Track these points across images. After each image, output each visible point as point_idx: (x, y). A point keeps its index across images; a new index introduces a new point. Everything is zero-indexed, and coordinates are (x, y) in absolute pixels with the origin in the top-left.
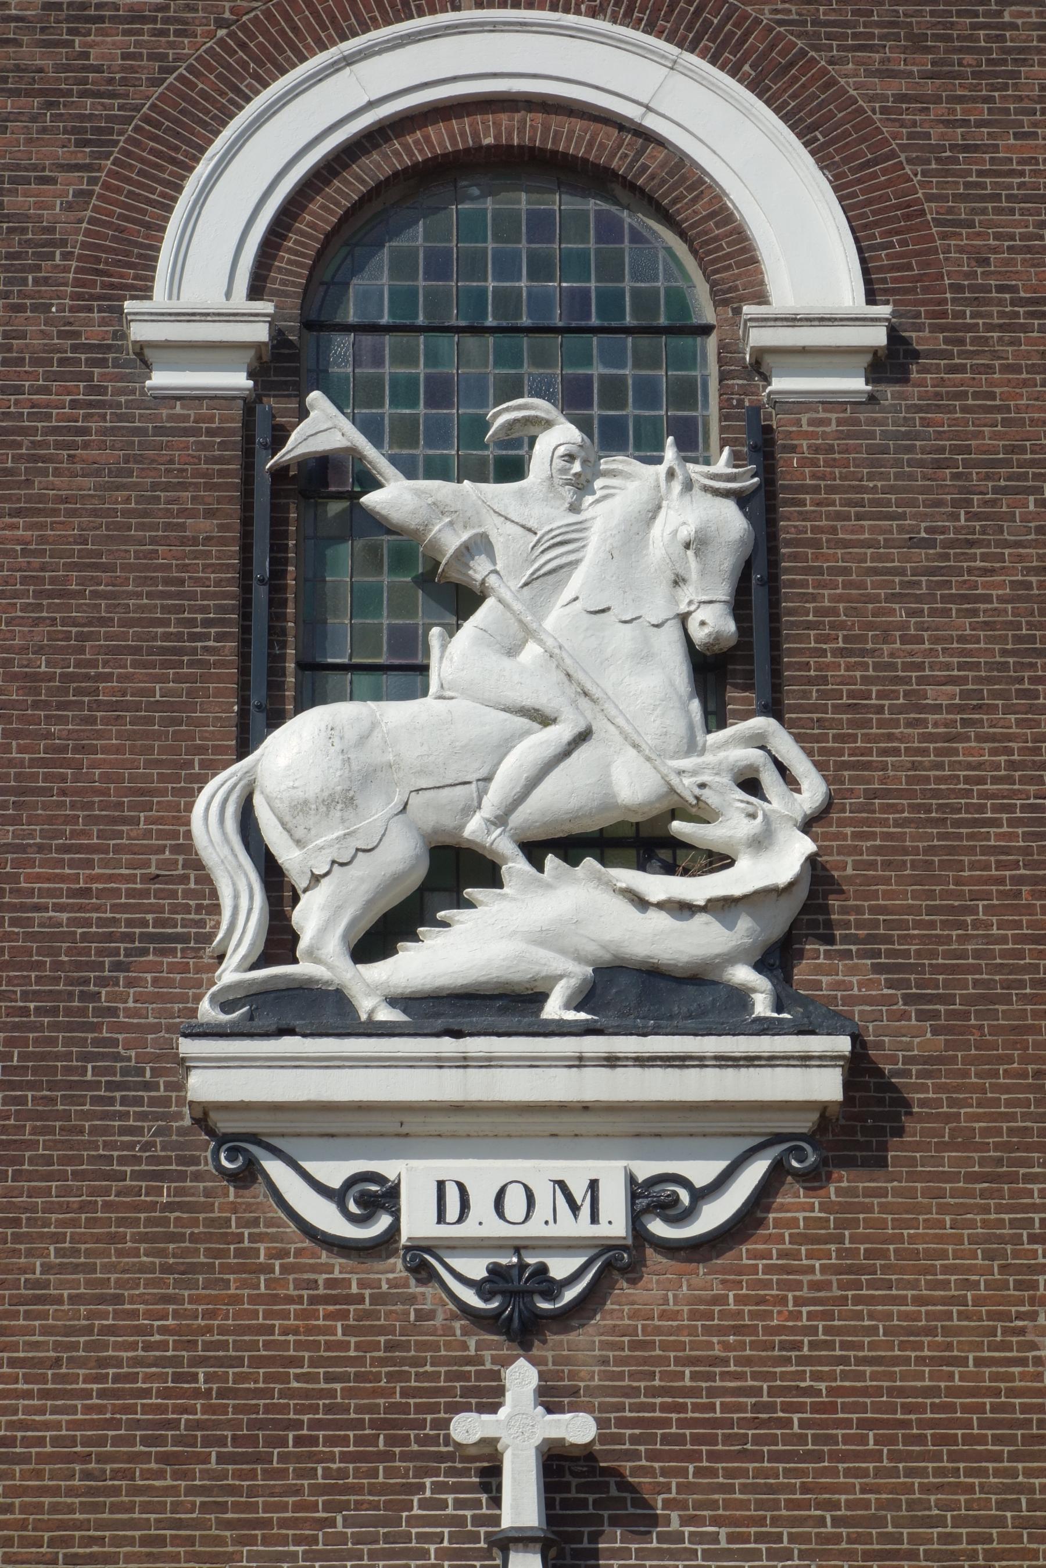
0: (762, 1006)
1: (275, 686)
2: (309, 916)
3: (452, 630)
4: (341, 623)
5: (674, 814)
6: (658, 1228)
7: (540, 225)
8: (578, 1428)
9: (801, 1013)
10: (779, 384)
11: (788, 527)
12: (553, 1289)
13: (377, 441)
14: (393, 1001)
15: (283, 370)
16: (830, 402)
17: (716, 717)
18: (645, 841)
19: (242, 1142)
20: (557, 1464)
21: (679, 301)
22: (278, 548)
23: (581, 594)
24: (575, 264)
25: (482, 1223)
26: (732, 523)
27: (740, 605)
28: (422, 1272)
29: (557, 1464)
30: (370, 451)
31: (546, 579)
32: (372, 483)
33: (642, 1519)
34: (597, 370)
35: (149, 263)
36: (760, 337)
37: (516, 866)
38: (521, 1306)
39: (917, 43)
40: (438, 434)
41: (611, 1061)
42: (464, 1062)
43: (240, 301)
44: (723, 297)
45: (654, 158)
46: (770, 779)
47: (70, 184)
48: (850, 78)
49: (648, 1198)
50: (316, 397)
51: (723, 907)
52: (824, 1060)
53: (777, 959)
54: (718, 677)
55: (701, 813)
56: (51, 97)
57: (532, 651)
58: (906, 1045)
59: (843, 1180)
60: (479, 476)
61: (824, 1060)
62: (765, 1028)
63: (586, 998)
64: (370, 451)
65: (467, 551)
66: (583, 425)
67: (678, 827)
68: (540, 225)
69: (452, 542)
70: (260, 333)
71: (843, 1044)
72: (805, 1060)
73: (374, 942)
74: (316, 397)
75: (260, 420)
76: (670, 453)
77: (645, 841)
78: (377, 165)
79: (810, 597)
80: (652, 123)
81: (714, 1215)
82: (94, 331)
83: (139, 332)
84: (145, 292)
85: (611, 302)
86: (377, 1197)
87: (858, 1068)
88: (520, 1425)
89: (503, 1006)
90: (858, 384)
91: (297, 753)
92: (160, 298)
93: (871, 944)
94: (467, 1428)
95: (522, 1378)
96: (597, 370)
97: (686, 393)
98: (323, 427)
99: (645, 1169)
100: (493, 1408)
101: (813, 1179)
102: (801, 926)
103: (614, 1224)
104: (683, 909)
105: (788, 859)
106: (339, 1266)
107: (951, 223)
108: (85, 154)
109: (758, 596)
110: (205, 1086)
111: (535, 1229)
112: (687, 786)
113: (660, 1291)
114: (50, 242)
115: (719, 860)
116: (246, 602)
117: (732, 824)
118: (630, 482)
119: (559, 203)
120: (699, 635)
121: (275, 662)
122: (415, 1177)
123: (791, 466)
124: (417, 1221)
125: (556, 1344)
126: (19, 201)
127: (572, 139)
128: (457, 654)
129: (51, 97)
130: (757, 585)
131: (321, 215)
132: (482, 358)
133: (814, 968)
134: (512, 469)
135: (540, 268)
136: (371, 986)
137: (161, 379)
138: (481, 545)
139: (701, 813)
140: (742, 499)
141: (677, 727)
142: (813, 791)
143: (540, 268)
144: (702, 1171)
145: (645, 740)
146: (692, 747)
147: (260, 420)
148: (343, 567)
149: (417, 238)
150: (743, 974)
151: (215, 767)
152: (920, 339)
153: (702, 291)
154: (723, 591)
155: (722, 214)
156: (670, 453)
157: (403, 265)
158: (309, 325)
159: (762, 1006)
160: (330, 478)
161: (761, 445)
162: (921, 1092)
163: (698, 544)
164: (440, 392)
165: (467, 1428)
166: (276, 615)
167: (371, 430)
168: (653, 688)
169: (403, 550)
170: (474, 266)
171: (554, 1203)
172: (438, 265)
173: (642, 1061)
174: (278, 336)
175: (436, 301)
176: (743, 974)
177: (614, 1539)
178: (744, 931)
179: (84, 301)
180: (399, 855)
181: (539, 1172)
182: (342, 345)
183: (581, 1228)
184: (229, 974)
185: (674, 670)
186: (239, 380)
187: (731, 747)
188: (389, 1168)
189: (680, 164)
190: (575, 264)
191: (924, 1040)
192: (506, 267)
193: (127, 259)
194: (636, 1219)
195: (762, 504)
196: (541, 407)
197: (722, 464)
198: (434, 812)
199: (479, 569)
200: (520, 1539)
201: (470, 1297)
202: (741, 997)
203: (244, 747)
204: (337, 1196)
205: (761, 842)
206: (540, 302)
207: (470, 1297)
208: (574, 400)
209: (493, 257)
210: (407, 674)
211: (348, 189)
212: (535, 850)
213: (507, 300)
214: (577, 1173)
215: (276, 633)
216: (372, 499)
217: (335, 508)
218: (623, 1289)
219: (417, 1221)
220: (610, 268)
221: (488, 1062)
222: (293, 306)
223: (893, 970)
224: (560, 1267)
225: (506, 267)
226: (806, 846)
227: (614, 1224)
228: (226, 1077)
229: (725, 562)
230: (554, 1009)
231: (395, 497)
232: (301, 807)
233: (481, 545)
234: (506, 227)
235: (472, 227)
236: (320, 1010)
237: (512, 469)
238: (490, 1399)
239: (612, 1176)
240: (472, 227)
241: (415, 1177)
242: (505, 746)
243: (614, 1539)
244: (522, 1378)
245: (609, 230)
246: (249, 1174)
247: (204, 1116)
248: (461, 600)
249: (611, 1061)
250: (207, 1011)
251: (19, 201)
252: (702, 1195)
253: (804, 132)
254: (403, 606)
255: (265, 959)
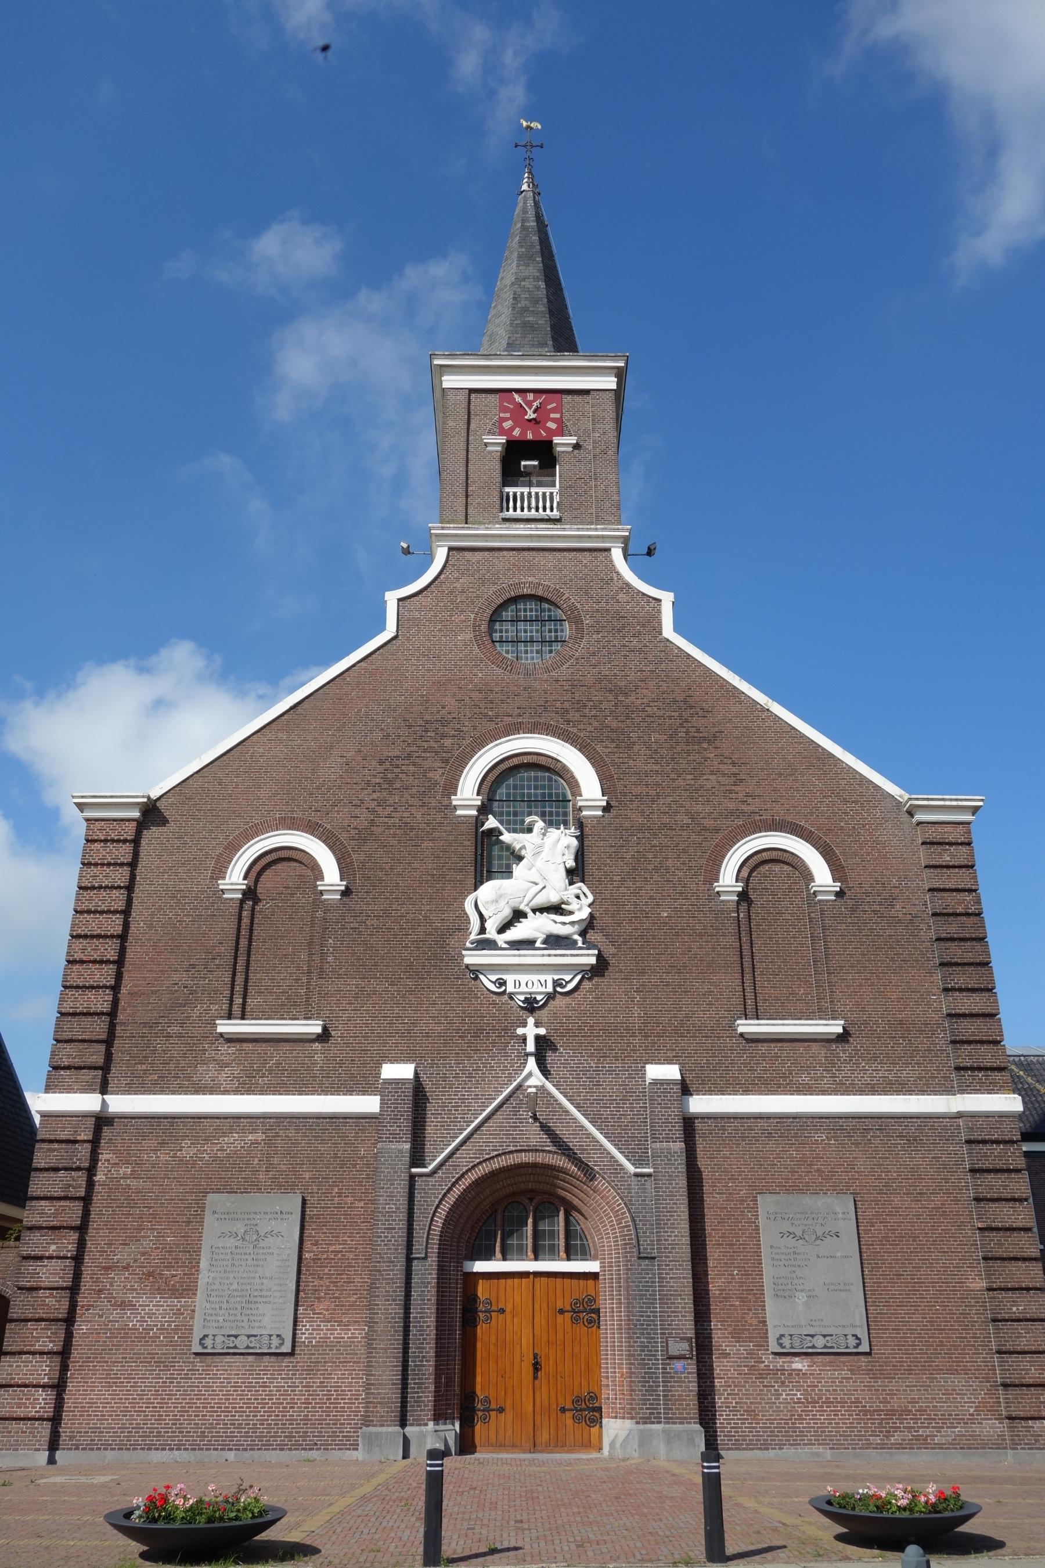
0: (580, 944)
1: (482, 876)
2: (488, 925)
3: (517, 864)
4: (495, 862)
5: (563, 903)
6: (559, 989)
7: (536, 779)
8: (542, 1031)
9: (589, 945)
10: (584, 813)
11: (586, 843)
12: (537, 1002)
13: (502, 824)
14: (506, 942)
15: (484, 810)
16: (595, 817)
17: (571, 883)
18: (557, 909)
19: (475, 972)
20: (538, 1038)
21: (564, 795)
22: (482, 847)
23: (544, 856)
24: (543, 787)
25: (523, 989)
26: (575, 842)
27: (576, 860)
28: (511, 998)
29: (538, 1038)
30: (501, 828)
31: (537, 854)
32: (501, 834)
33: (555, 1049)
34: (547, 809)
35: (456, 788)
36: (580, 804)
37: (530, 914)
38: (531, 1006)
39: (613, 741)
40: (515, 823)
41: (549, 955)
42: (520, 955)
43: (475, 796)
44: (574, 795)
45: (559, 765)
46: (582, 896)
47: (440, 771)
48: (599, 748)
49: (557, 983)
50: (490, 816)
51: (572, 923)
52: (593, 955)
53: (583, 934)
54: (574, 874)
55: (568, 904)
56: (437, 753)
57: (534, 869)
58: (609, 951)
59: (596, 979)
60: (523, 832)
61: (593, 955)
62: (581, 948)
63: (544, 942)
64: (501, 828)
65: (521, 849)
66: (544, 821)
67: (563, 906)
68: (536, 779)
69: (518, 847)
70: (479, 803)
71: (596, 952)
72: (588, 955)
73: (501, 930)
74: (490, 816)
75: (479, 822)
76: (562, 827)
77: (557, 909)
78: (503, 767)
79: (590, 858)
80: (558, 758)
81: (570, 987)
82: (445, 802)
83: (454, 803)
84: (455, 795)
85: (550, 795)
86: (502, 983)
87: (599, 957)
88: (530, 1030)
89: (527, 944)
90: (600, 813)
91: (488, 891)
92: (459, 796)
93: (602, 930)
94: (520, 1031)
95: (531, 1021)
96: (547, 809)
97: (565, 814)
98: (492, 822)
99: (556, 977)
100: (525, 1026)
101: (590, 979)
102: (588, 927)
103: (550, 989)
104: (564, 924)
105: (584, 913)
106: (494, 997)
107: (619, 779)
108: (443, 765)
109: (580, 857)
110: (467, 960)
111: (534, 990)
112: (565, 898)
113: (559, 1002)
114: (436, 783)
115: (571, 913)
116: (476, 859)
117: (574, 906)
118: (554, 833)
119: (540, 774)
120: (568, 866)
121: (482, 871)
122: (510, 978)
123: (587, 830)
124: (510, 988)
125: (538, 1013)
126: (430, 775)
127: (542, 761)
128: (518, 870)
129: (437, 753)
130: (580, 855)
131: (491, 777)
132: (524, 807)
133: (591, 936)
134: (530, 830)
135: (536, 788)
136: (501, 939)
137: (459, 812)
138: (524, 847)
139: (568, 904)
140: (576, 837)
141: (563, 886)
142: (591, 898)
143: (536, 788)
144: (568, 978)
145: (557, 889)
146: (566, 889)
147: (479, 822)
148: (496, 851)
149: (511, 781)
150: (576, 937)
151: (470, 893)
152: (613, 803)
153: (569, 792)
154: (573, 857)
155: (573, 777)
156: (562, 827)
157: (508, 787)
158: (489, 800)
159: (580, 944)
160: (493, 832)
161: (580, 825)
162: (612, 961)
163: (568, 847)
164: (515, 814)
165: (520, 1031)
166: (482, 861)
167: (501, 822)
168: (559, 877)
169: (508, 847)
170: (522, 787)
171: (539, 985)
172: (515, 787)
173: (556, 955)
174: (483, 803)
175: (515, 795)
176: (576, 937)
177: (549, 1053)
178: (576, 928)
179: (443, 796)
180: (507, 913)
181: (535, 978)
182: (496, 804)
183: (543, 989)
184: (473, 937)
185: (563, 873)
186: (475, 813)
187: (574, 889)
188: (504, 977)
189: (564, 766)
190: (543, 787)
191: (613, 950)
192: (529, 788)
193: (451, 787)
194: (554, 988)
195: (581, 838)
196: (536, 818)
197: (573, 830)
198: (514, 903)
199: (523, 853)
200: (531, 1054)
201: (521, 1004)
202: (575, 942)
203: (476, 889)
204: (494, 983)
205: (580, 909)
206: (536, 795)
207: (521, 1004)
208: (543, 815)
209: (529, 789)
210: (508, 873)
211: (497, 772)
212: (534, 911)
213: (529, 795)
214: (542, 978)
215: (482, 865)
216: (501, 838)
217: (494, 838)
218: (551, 1002)
219: (510, 988)
220: (550, 788)
221: (525, 955)
222: (486, 797)
223: (607, 936)
224: (539, 997)
225: (529, 788)
226: (589, 910)
227: (550, 989)
228: (472, 958)
229: (573, 851)
230: (538, 944)
231: (507, 837)
232: (487, 902)
233: (524, 847)
234: (529, 779)
235: (522, 779)
236: (488, 944)
237: (530, 830)
238: (524, 1024)
239: (549, 978)
240: (522, 779)
241: (510, 978)
242: (528, 890)
243: (549, 1053)
244: (531, 1021)
245: (550, 779)
246: (476, 978)
247: (467, 966)
248: (520, 858)
249: (549, 955)
250: (468, 945)
251: (430, 775)
252: (567, 983)
253: (589, 760)
254: (508, 859)
255: (479, 934)
